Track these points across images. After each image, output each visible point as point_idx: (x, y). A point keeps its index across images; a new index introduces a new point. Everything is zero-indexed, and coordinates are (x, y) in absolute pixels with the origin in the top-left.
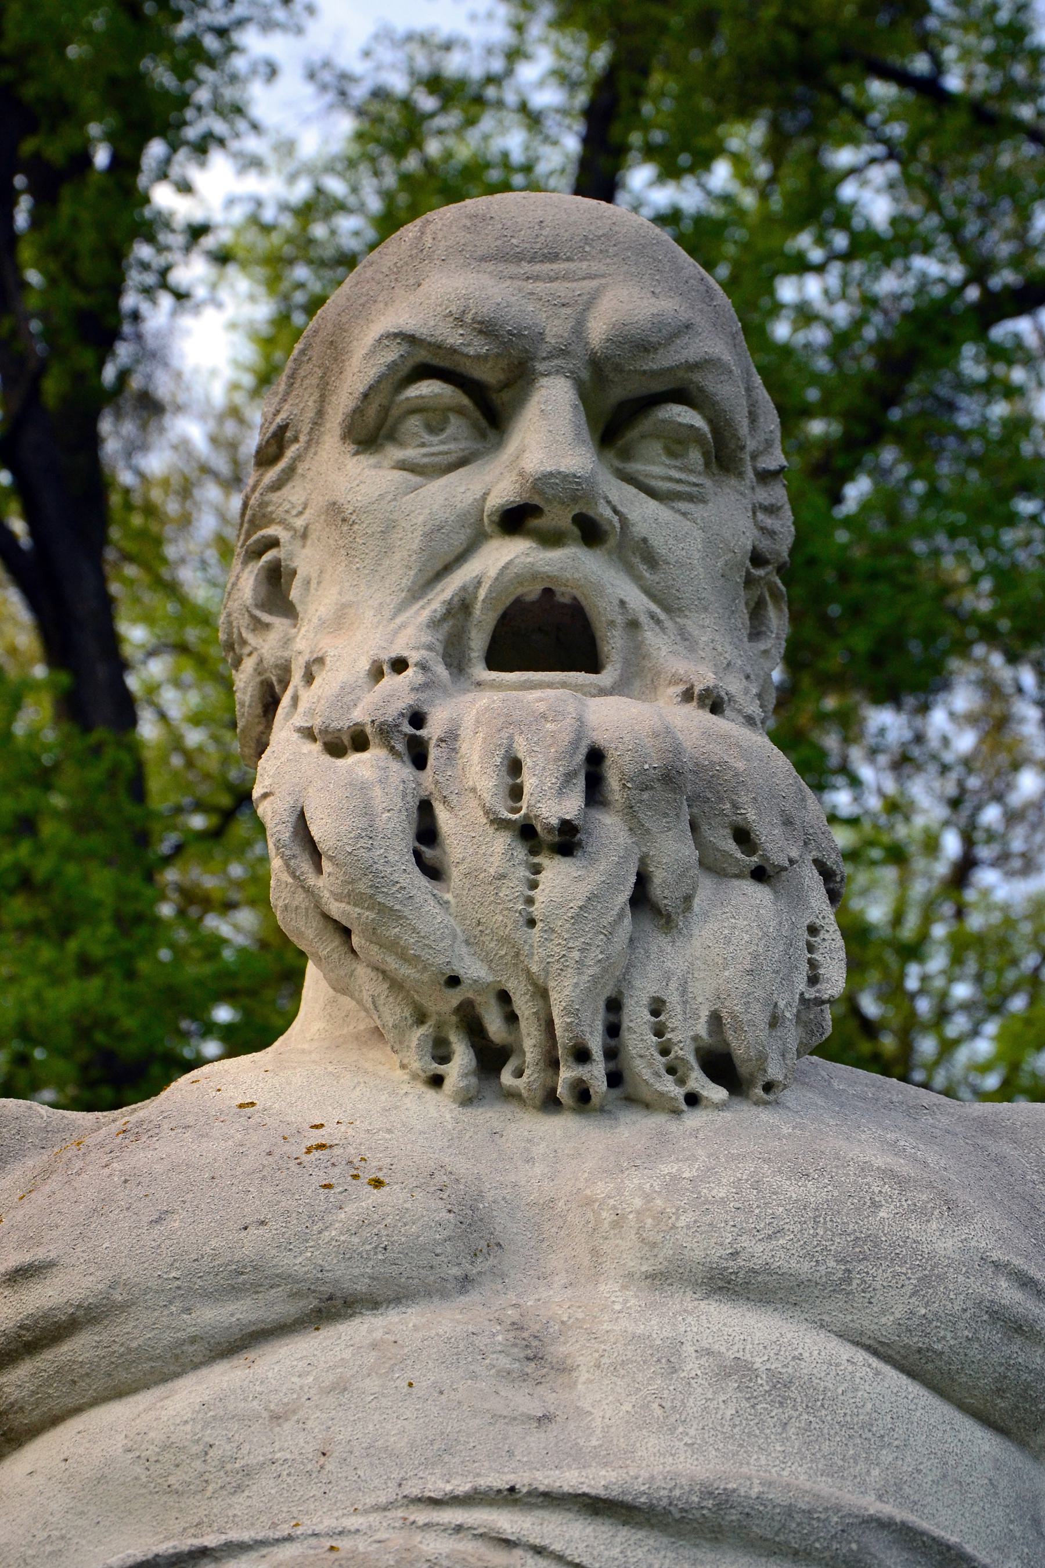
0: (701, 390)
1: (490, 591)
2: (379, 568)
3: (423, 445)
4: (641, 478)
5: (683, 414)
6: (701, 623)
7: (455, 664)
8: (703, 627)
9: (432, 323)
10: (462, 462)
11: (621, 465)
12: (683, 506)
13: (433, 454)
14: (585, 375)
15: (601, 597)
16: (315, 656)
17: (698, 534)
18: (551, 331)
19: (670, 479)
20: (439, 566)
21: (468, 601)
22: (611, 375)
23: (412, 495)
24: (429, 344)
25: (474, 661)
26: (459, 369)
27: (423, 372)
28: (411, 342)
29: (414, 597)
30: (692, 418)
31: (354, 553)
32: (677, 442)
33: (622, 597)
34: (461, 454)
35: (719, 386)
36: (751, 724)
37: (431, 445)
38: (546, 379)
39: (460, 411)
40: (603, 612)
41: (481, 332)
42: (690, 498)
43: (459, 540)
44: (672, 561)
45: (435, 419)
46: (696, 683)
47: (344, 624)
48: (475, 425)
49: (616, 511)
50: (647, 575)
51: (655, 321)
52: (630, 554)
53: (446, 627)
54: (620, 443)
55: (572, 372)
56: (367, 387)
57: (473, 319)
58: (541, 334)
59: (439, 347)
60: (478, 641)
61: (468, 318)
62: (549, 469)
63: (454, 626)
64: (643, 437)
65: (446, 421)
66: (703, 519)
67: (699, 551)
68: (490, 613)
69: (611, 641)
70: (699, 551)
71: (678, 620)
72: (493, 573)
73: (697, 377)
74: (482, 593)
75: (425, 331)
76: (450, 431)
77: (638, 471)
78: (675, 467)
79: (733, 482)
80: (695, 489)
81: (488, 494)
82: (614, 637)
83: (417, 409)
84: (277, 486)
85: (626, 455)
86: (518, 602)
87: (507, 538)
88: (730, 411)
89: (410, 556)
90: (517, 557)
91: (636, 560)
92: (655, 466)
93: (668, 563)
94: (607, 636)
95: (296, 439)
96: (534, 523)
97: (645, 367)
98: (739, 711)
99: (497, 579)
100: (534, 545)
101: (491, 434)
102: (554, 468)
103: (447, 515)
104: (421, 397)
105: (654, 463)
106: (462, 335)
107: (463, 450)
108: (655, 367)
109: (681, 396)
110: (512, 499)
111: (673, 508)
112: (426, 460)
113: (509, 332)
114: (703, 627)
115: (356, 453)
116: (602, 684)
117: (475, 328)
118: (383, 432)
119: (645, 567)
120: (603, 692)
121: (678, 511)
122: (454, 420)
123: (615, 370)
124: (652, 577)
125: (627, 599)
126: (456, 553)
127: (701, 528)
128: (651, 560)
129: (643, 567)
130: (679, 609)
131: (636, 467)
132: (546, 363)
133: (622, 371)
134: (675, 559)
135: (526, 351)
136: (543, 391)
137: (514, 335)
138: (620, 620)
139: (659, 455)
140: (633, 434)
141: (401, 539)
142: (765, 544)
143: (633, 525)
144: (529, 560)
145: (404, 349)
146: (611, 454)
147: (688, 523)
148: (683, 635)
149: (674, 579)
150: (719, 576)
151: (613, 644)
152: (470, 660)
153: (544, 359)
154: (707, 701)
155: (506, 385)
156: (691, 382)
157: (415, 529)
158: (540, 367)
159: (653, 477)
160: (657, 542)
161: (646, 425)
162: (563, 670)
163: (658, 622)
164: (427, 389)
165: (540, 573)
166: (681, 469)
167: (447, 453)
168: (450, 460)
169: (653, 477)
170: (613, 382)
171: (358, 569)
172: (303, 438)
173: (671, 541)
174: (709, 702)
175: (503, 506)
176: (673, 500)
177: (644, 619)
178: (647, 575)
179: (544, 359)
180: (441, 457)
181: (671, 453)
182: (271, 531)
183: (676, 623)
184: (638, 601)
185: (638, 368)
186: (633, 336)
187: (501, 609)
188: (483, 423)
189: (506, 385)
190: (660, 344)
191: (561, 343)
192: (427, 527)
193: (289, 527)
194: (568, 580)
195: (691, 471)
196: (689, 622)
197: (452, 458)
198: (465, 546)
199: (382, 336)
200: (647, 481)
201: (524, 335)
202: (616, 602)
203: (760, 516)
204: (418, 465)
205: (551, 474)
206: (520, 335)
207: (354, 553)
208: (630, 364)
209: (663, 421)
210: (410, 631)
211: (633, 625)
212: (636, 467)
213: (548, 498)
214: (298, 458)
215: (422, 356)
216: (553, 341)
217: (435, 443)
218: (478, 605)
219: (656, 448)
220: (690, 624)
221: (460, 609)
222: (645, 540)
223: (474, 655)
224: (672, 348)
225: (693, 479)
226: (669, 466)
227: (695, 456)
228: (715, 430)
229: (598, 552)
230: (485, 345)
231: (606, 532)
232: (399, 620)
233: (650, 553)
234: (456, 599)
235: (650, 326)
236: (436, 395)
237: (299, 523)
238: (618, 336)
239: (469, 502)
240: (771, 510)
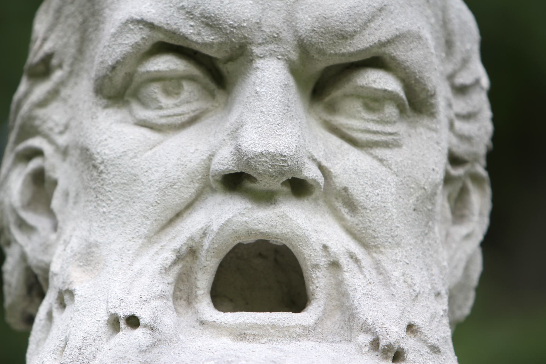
0: (393, 59)
1: (212, 243)
2: (122, 215)
3: (161, 108)
4: (344, 130)
5: (377, 80)
6: (394, 257)
7: (184, 297)
8: (396, 261)
9: (168, 13)
10: (193, 121)
11: (328, 118)
12: (380, 152)
13: (169, 116)
14: (294, 56)
15: (307, 246)
16: (66, 287)
17: (392, 178)
18: (265, 21)
19: (369, 131)
20: (170, 214)
21: (194, 248)
22: (316, 56)
23: (150, 153)
24: (166, 31)
25: (200, 297)
26: (190, 47)
27: (162, 48)
28: (150, 27)
29: (150, 242)
30: (386, 83)
31: (101, 197)
32: (374, 101)
33: (324, 242)
34: (192, 114)
35: (409, 54)
36: (435, 352)
37: (167, 108)
38: (262, 61)
39: (191, 78)
40: (310, 256)
41: (207, 25)
42: (386, 145)
43: (188, 193)
44: (369, 207)
45: (170, 83)
46: (381, 337)
47: (91, 261)
48: (205, 88)
49: (321, 167)
50: (348, 217)
51: (352, 13)
52: (333, 199)
53: (176, 269)
54: (327, 99)
55: (282, 55)
56: (114, 62)
57: (201, 14)
58: (258, 23)
59: (174, 33)
60: (204, 282)
61: (197, 13)
62: (259, 150)
63: (184, 266)
64: (346, 96)
65: (180, 87)
66: (397, 163)
67: (392, 194)
68: (213, 259)
69: (316, 282)
70: (392, 194)
71: (375, 255)
72: (215, 228)
73: (390, 50)
74: (207, 243)
75: (162, 19)
76: (184, 95)
77: (342, 125)
78: (373, 121)
79: (426, 121)
80: (390, 137)
81: (213, 156)
82: (318, 277)
83: (158, 78)
84: (43, 103)
85: (332, 108)
86: (239, 245)
87: (228, 196)
88: (419, 72)
89: (147, 208)
90: (235, 216)
91: (339, 205)
92: (356, 120)
93: (365, 208)
94: (312, 277)
95: (60, 66)
96: (249, 185)
97: (344, 51)
98: (425, 342)
99: (218, 233)
100: (249, 206)
101: (220, 95)
102: (264, 148)
103: (178, 173)
104: (158, 71)
105: (355, 117)
106: (191, 26)
107: (194, 111)
108: (352, 50)
109: (376, 61)
110: (231, 168)
111: (371, 154)
112: (163, 121)
113: (231, 26)
114: (396, 261)
115: (106, 107)
116: (305, 324)
117: (203, 22)
118: (129, 91)
119: (347, 210)
120: (307, 332)
121: (376, 157)
122: (187, 86)
123: (319, 53)
124: (353, 219)
125: (329, 244)
126: (186, 204)
127: (395, 173)
128: (352, 205)
129: (344, 211)
130: (375, 246)
131: (340, 120)
132: (262, 48)
133: (324, 54)
134: (371, 204)
135: (245, 38)
136: (259, 73)
137: (235, 28)
138: (323, 261)
139: (359, 112)
140: (337, 93)
141: (140, 192)
142: (461, 149)
143: (335, 177)
144: (245, 219)
145: (146, 32)
146: (319, 108)
147: (384, 168)
148: (379, 268)
149: (370, 222)
150: (411, 211)
151: (319, 283)
152: (196, 297)
153: (260, 44)
154: (389, 354)
155: (231, 59)
156: (384, 53)
157: (152, 185)
158: (257, 50)
159: (354, 130)
160: (357, 191)
161: (347, 88)
162: (271, 311)
163: (357, 261)
164: (165, 64)
165: (254, 230)
166: (377, 122)
167: (180, 115)
168: (183, 120)
169: (354, 130)
170: (318, 60)
171: (104, 212)
172: (66, 68)
173: (368, 189)
174: (391, 355)
175: (224, 172)
176: (371, 147)
177: (344, 260)
178: (348, 217)
179: (260, 44)
180: (175, 118)
181: (368, 108)
182: (36, 142)
183: (373, 258)
184: (339, 242)
185: (337, 52)
186: (333, 27)
187: (222, 256)
188: (212, 86)
189: (231, 59)
190: (355, 32)
191: (274, 32)
192: (162, 184)
193: (51, 142)
194: (277, 235)
195: (387, 123)
196: (384, 258)
197: (185, 118)
198: (194, 196)
199: (128, 20)
200: (349, 133)
201: (244, 27)
202: (319, 248)
203: (459, 125)
204: (157, 125)
205: (262, 154)
206: (240, 27)
207: (101, 197)
208: (331, 49)
209: (362, 87)
210: (145, 280)
211: (335, 265)
212: (340, 120)
213: (259, 173)
214: (62, 83)
215: (160, 37)
216: (268, 30)
217: (170, 106)
218: (203, 253)
219: (357, 106)
220: (386, 259)
221: (190, 253)
222: (345, 189)
223: (200, 292)
224: (366, 32)
225: (389, 129)
226: (368, 121)
227: (391, 110)
228: (408, 88)
229: (306, 201)
230: (212, 34)
231: (312, 186)
232: (137, 266)
233: (349, 199)
234: (184, 248)
235: (347, 18)
236: (171, 71)
237: (62, 140)
238: (321, 27)
239: (198, 162)
240: (468, 117)
